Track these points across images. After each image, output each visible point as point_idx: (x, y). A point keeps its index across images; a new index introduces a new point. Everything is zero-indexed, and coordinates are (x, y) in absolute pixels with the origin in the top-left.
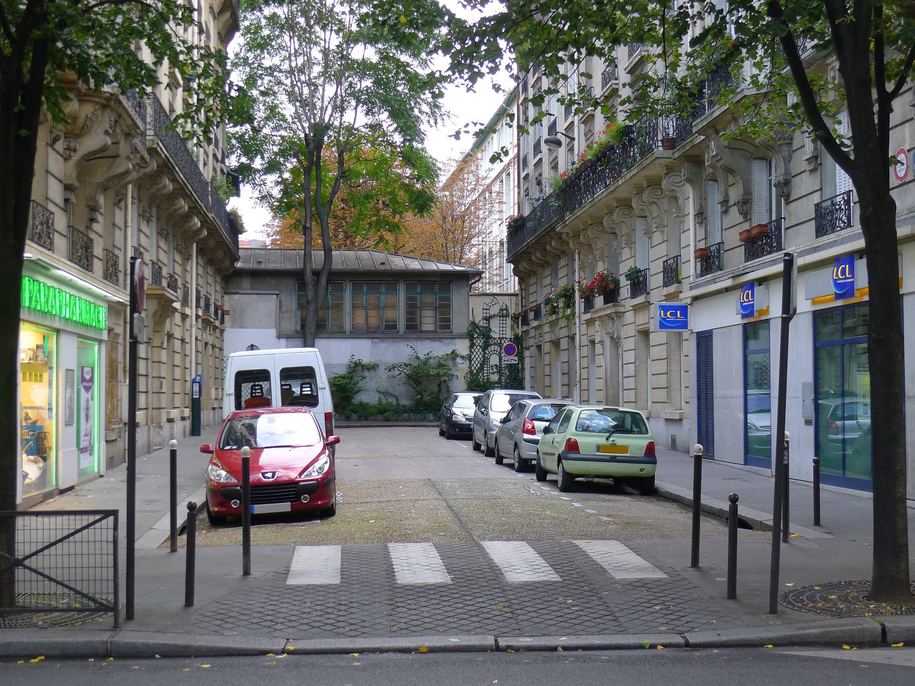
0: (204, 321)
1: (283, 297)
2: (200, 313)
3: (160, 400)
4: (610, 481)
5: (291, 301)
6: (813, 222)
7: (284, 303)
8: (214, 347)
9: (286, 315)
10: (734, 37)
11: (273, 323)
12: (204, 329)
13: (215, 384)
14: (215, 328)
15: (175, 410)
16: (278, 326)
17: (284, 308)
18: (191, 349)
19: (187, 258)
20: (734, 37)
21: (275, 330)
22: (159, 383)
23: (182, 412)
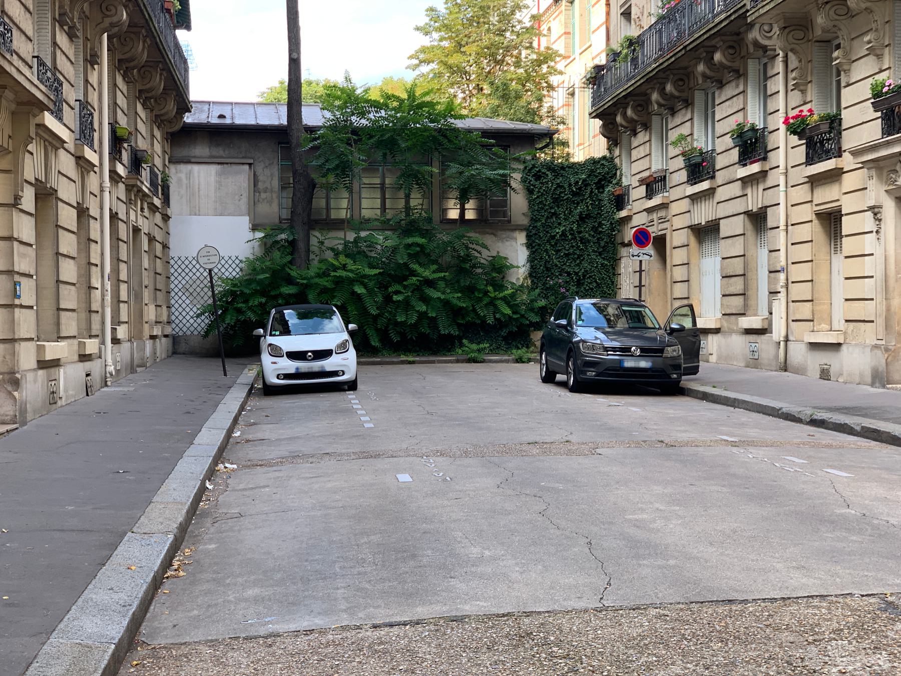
0: (129, 188)
1: (259, 168)
2: (121, 170)
3: (12, 323)
4: (18, 293)
5: (271, 176)
6: (717, 167)
7: (261, 178)
8: (152, 239)
9: (263, 195)
10: (439, 236)
11: (243, 203)
12: (129, 202)
13: (155, 299)
14: (153, 208)
15: (62, 344)
16: (252, 211)
17: (261, 186)
18: (100, 230)
19: (92, 60)
20: (439, 236)
21: (246, 219)
22: (9, 286)
23: (82, 345)
